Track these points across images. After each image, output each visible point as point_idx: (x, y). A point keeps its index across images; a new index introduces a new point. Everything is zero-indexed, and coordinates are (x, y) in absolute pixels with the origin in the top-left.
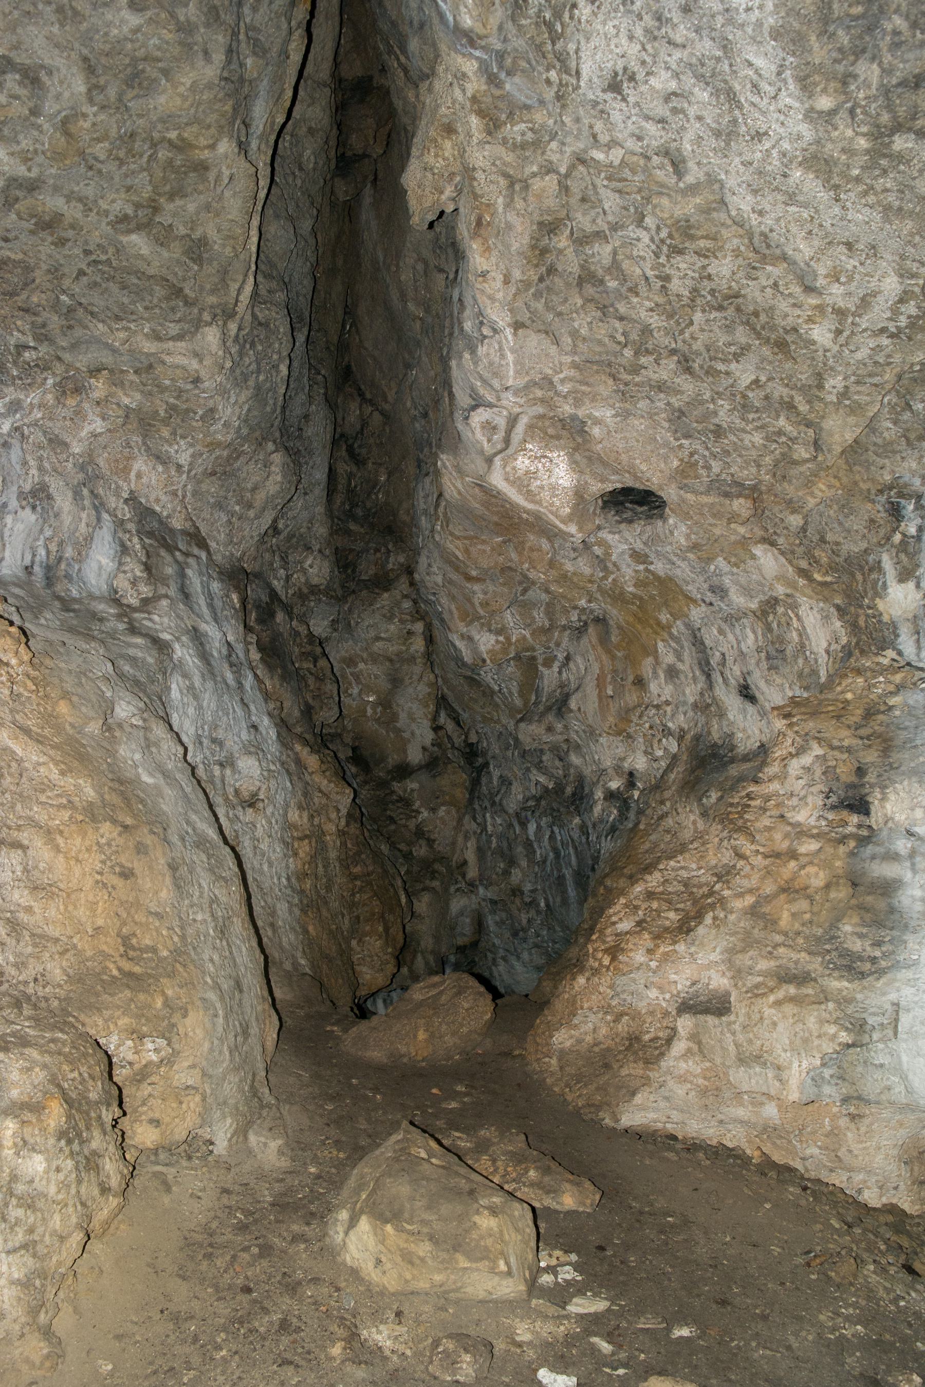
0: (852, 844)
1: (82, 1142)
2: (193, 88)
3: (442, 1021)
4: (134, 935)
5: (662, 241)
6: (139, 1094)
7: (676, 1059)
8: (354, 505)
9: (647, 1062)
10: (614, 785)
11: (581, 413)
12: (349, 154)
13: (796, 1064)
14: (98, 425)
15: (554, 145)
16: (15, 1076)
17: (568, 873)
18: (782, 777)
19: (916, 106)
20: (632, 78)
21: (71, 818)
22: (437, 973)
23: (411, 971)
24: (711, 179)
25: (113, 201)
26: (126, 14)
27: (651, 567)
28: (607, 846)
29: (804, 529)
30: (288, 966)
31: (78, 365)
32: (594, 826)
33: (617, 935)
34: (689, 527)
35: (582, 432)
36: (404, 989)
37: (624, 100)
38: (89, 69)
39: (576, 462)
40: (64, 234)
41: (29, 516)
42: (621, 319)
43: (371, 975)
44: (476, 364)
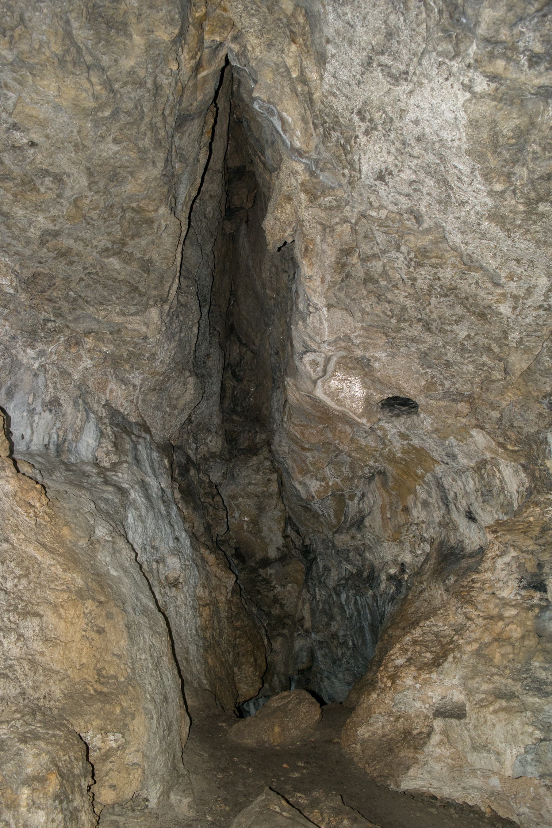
0: (537, 610)
1: (69, 802)
2: (146, 181)
3: (291, 720)
4: (104, 668)
5: (411, 259)
6: (104, 768)
7: (434, 746)
8: (236, 405)
9: (416, 748)
10: (392, 571)
11: (367, 355)
12: (232, 207)
13: (508, 752)
14: (88, 363)
15: (348, 208)
16: (30, 759)
17: (366, 625)
18: (493, 569)
19: (549, 189)
20: (390, 173)
21: (68, 597)
22: (285, 690)
23: (270, 685)
24: (438, 226)
25: (100, 241)
26: (111, 145)
27: (411, 442)
28: (389, 609)
29: (500, 419)
30: (195, 684)
31: (78, 330)
32: (381, 596)
33: (395, 667)
34: (433, 419)
35: (369, 366)
36: (267, 697)
37: (386, 184)
38: (90, 173)
39: (365, 383)
40: (72, 259)
41: (48, 416)
42: (389, 302)
43: (246, 689)
44: (306, 328)
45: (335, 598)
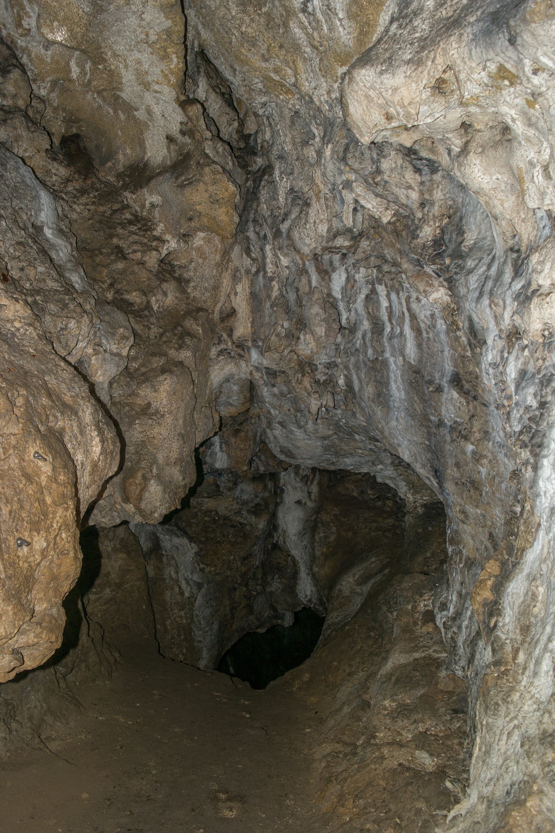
45: (315, 278)
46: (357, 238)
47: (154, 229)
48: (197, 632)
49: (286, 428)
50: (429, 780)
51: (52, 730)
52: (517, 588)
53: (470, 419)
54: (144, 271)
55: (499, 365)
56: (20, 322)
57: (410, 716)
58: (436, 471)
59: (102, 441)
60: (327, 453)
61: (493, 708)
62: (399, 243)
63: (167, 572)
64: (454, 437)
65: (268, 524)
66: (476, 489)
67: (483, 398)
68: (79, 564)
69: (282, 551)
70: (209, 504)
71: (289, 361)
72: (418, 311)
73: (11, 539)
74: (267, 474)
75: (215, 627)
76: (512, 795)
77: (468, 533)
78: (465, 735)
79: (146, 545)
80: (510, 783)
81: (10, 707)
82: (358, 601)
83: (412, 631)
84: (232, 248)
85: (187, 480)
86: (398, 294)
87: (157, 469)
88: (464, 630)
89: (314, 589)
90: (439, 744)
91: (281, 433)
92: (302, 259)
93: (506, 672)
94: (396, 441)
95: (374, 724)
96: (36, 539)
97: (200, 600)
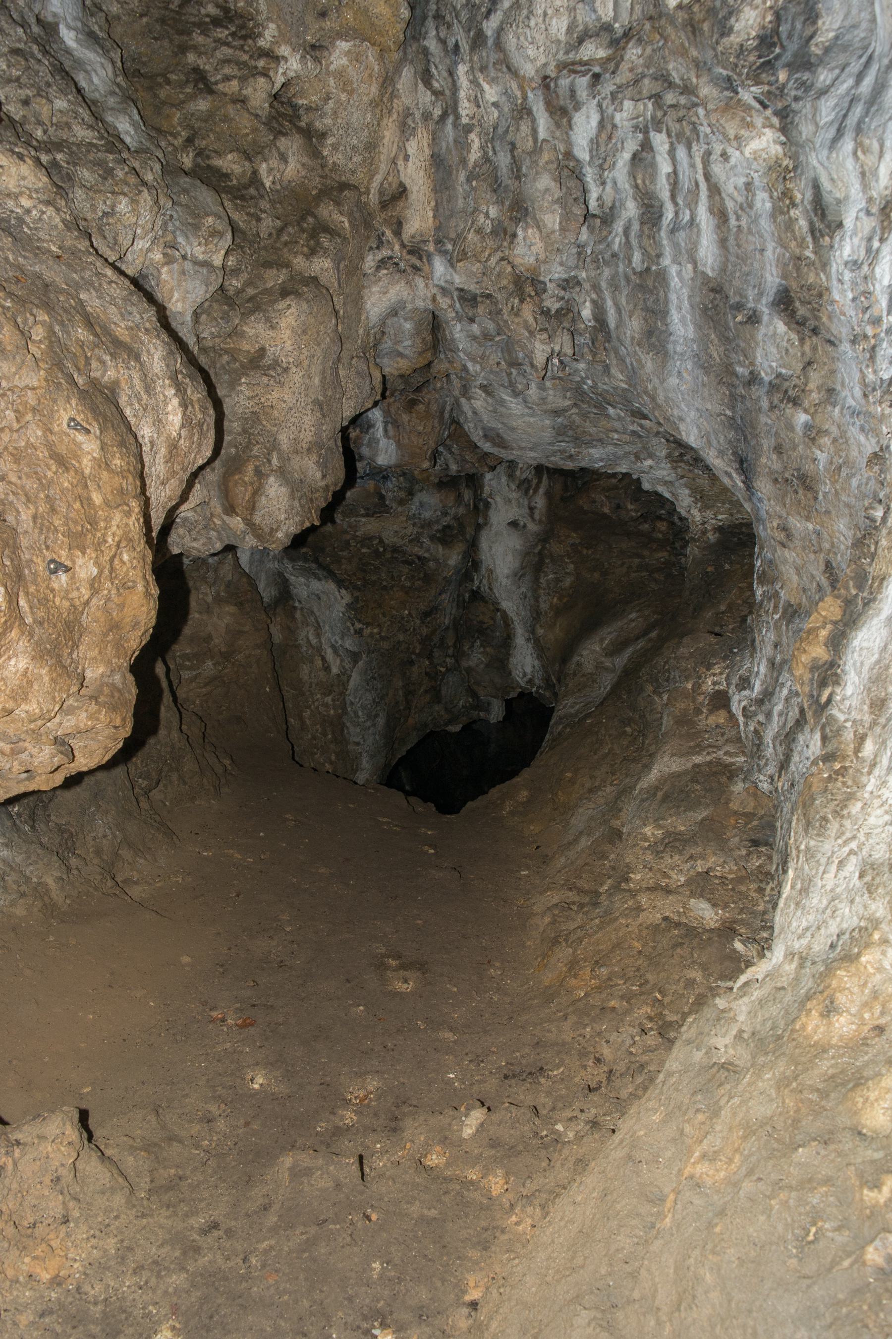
45: (543, 122)
46: (618, 41)
47: (260, 35)
48: (352, 729)
49: (493, 397)
50: (709, 939)
51: (132, 870)
52: (869, 640)
53: (804, 368)
54: (246, 115)
55: (862, 263)
56: (31, 197)
57: (684, 849)
58: (741, 462)
59: (184, 405)
60: (560, 438)
61: (818, 824)
62: (696, 47)
63: (303, 634)
64: (776, 402)
65: (464, 558)
66: (808, 488)
67: (828, 330)
68: (154, 604)
69: (486, 602)
70: (368, 526)
71: (499, 275)
72: (723, 178)
73: (39, 560)
74: (463, 476)
75: (381, 721)
76: (839, 948)
77: (788, 568)
78: (769, 876)
79: (267, 592)
80: (837, 931)
81: (66, 836)
82: (607, 681)
83: (691, 723)
84: (398, 70)
85: (329, 480)
86: (689, 148)
87: (278, 459)
88: (775, 718)
89: (536, 663)
90: (727, 890)
91: (484, 405)
92: (521, 88)
93: (842, 771)
94: (676, 412)
95: (628, 860)
96: (80, 561)
97: (355, 679)
